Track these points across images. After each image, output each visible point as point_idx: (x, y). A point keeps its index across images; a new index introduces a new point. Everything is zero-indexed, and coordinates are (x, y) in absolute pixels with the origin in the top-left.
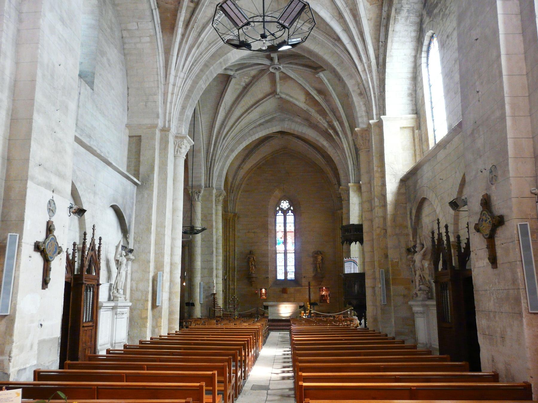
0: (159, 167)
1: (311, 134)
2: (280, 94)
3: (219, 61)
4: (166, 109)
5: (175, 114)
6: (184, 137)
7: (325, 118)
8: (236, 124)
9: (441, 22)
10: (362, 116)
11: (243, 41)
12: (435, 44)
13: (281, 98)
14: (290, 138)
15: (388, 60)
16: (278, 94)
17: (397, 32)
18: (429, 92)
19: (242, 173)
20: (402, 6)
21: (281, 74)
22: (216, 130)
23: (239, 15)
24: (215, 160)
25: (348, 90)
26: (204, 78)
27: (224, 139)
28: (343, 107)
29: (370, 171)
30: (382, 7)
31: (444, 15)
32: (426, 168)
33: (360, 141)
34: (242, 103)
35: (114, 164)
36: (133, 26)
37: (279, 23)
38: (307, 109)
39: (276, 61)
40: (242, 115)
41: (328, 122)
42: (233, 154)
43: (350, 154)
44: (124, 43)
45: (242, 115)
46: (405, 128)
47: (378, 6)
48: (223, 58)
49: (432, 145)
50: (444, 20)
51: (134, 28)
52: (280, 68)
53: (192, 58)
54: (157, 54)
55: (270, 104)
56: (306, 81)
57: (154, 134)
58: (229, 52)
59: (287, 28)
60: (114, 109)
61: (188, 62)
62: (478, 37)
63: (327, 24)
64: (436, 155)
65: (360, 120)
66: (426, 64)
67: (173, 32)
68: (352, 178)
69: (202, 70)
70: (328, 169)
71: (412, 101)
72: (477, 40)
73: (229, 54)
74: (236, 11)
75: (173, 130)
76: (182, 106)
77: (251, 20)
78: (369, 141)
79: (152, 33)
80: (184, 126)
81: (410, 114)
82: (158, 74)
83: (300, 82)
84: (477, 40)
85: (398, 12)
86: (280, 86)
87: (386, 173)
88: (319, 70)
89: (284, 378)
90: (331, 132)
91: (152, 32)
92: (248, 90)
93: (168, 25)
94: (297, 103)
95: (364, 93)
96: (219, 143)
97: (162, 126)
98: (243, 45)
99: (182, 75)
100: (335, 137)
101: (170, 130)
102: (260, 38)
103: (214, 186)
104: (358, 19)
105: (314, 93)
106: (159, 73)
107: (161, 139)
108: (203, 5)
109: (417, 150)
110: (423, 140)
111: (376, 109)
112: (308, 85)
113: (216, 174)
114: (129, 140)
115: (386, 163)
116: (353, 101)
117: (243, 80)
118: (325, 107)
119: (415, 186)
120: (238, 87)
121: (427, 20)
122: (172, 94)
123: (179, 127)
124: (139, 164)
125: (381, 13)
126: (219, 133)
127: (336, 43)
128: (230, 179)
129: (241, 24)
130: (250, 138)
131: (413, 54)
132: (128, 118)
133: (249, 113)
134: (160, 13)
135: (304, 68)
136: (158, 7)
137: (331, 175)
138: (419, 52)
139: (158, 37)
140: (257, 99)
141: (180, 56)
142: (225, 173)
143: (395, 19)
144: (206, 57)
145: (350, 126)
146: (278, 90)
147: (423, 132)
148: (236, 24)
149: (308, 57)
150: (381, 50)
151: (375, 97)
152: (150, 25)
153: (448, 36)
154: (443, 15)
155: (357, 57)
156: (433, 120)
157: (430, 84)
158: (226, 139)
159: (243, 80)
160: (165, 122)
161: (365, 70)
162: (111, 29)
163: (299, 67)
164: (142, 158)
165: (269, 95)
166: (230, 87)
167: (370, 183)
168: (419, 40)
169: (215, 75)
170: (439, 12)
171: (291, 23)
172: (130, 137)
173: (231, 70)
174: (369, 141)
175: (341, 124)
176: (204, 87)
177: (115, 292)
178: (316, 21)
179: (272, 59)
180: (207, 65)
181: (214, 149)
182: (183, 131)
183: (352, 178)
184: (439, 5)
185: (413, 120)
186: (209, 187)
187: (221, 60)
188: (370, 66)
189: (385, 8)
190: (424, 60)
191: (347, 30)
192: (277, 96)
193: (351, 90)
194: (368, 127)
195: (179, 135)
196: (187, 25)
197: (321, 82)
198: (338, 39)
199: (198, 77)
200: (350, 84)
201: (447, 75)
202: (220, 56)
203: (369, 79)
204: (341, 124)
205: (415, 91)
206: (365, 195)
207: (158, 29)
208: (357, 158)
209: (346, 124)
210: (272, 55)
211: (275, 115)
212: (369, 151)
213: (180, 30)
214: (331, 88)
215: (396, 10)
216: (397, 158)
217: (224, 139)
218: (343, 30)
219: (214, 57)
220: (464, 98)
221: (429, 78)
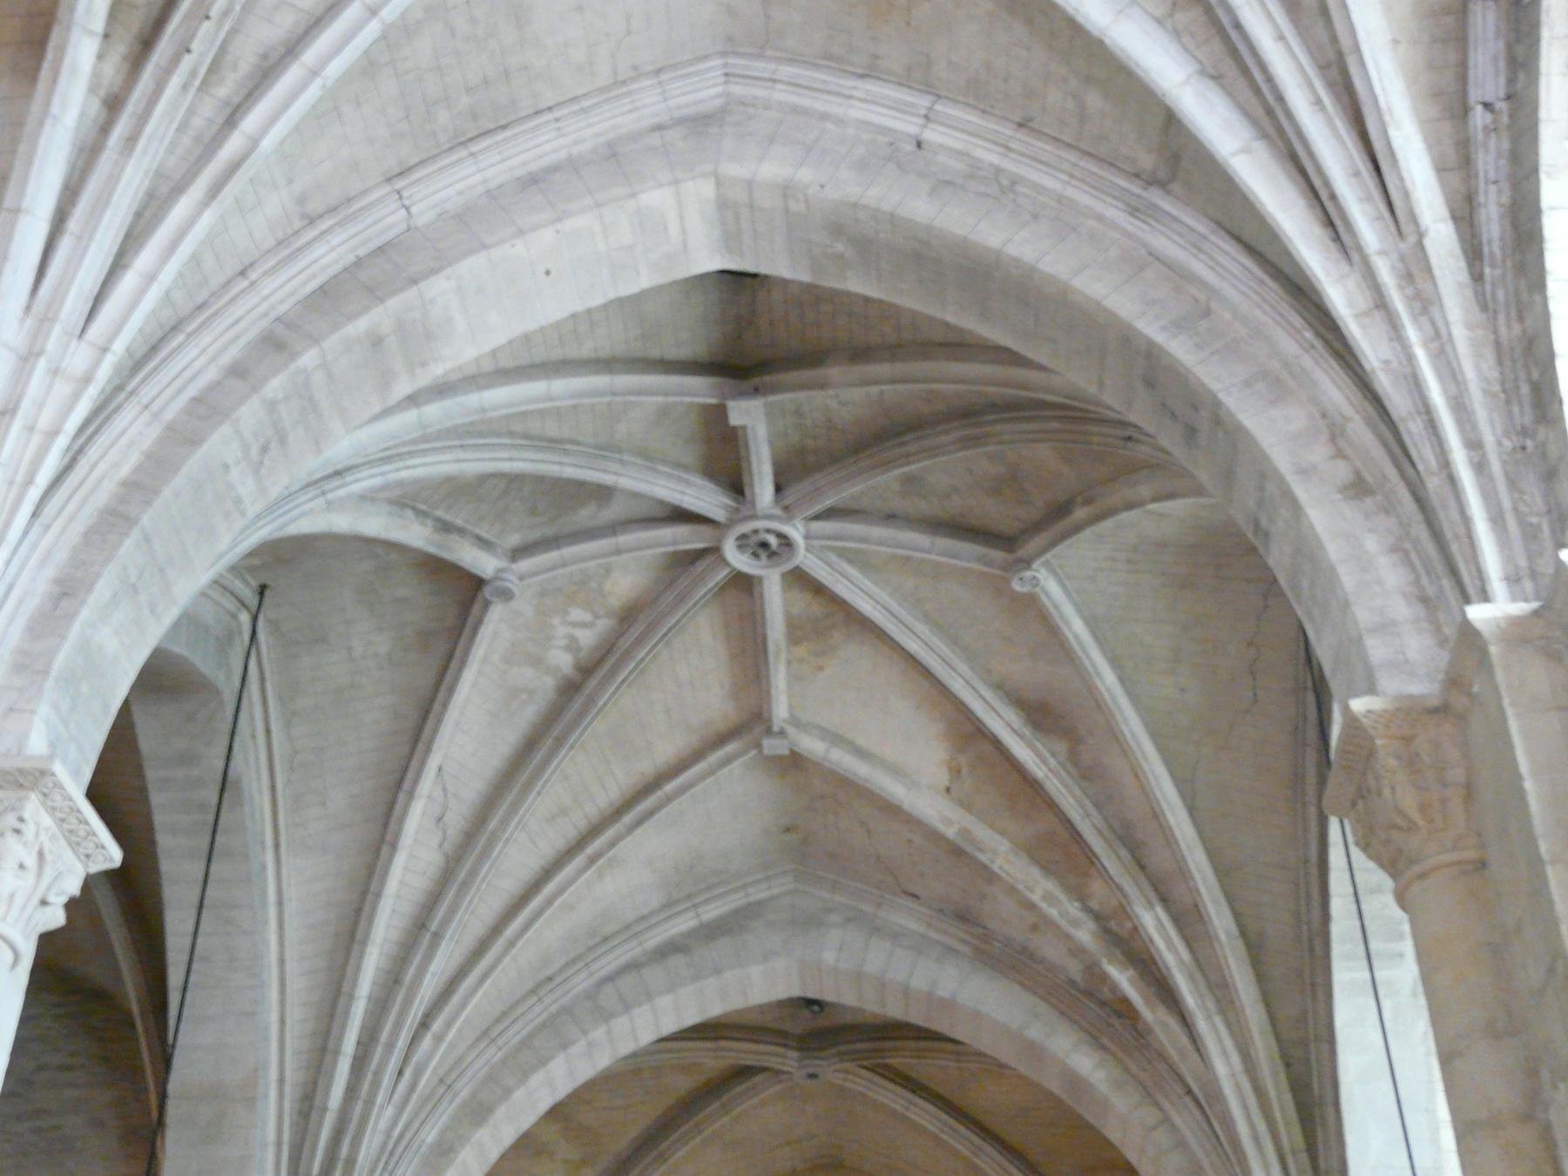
2: (790, 730)
3: (361, 326)
8: (510, 931)
10: (1386, 627)
16: (782, 733)
21: (803, 603)
27: (424, 1025)
28: (1192, 810)
38: (964, 832)
39: (763, 491)
40: (547, 874)
41: (1098, 917)
42: (483, 1134)
43: (1261, 1126)
45: (547, 874)
48: (393, 303)
55: (726, 811)
56: (954, 641)
67: (37, 69)
76: (58, 581)
80: (44, 709)
83: (913, 646)
86: (795, 679)
90: (1123, 979)
92: (591, 700)
94: (896, 790)
96: (390, 1046)
100: (1147, 1014)
105: (1004, 723)
112: (963, 668)
117: (561, 631)
120: (524, 675)
126: (393, 980)
130: (598, 1034)
135: (944, 543)
140: (646, 767)
141: (73, 225)
145: (1243, 933)
146: (780, 710)
151: (1480, 467)
158: (436, 1026)
165: (721, 740)
166: (469, 675)
175: (1188, 920)
188: (1416, 268)
194: (1454, 682)
202: (375, 294)
204: (1188, 920)
217: (424, 1025)
218: (1203, 72)
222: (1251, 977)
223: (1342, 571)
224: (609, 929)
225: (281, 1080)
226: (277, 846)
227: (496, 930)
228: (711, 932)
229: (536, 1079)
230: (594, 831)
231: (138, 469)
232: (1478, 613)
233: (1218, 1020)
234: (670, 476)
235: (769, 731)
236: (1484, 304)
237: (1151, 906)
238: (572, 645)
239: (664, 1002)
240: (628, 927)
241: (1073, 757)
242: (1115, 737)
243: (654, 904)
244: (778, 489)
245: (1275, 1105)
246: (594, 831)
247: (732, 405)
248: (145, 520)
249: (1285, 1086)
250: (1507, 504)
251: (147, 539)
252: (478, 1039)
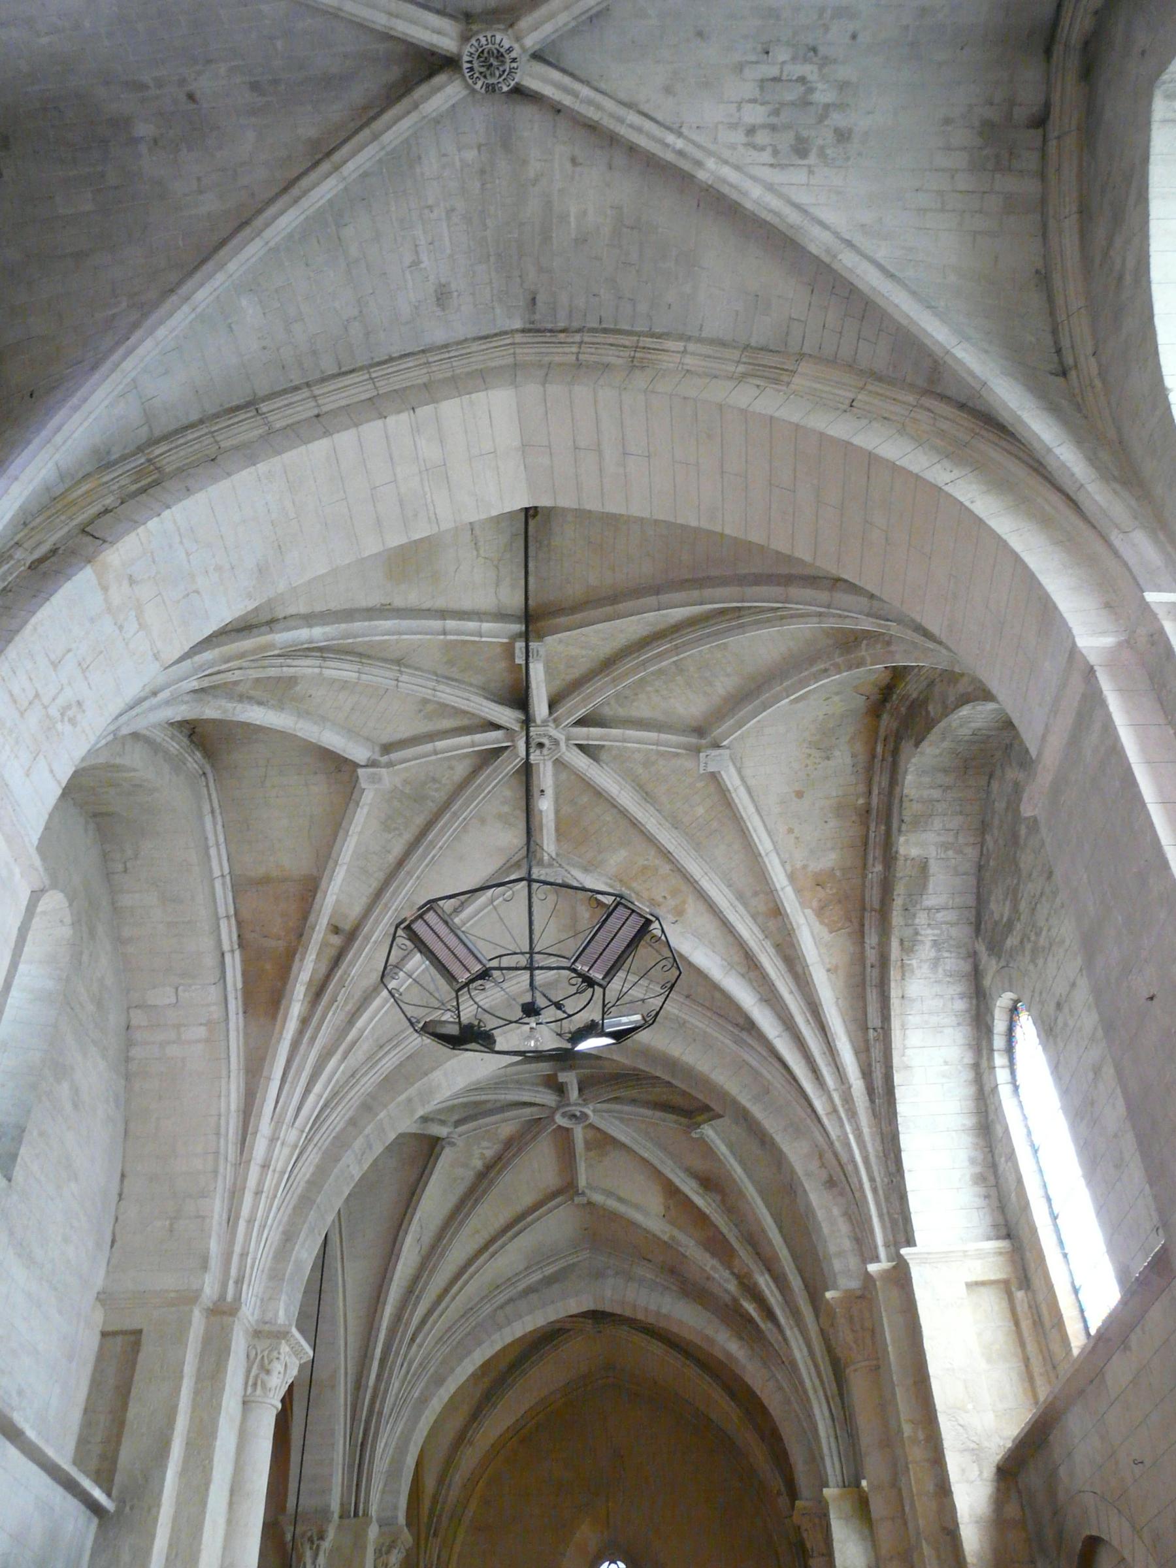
0: (189, 1444)
1: (687, 1318)
2: (587, 1191)
3: (404, 1096)
4: (231, 1242)
5: (261, 1253)
6: (282, 1335)
7: (729, 1267)
9: (1031, 967)
10: (841, 1254)
11: (470, 1026)
12: (1027, 1029)
13: (589, 1203)
14: (623, 1332)
15: (898, 1078)
16: (583, 1194)
17: (913, 1000)
18: (1035, 1168)
19: (470, 1458)
20: (917, 933)
21: (591, 1134)
22: (388, 1311)
23: (461, 951)
24: (380, 1413)
25: (793, 1172)
26: (358, 1143)
27: (413, 1340)
28: (780, 1228)
29: (890, 1441)
30: (863, 936)
31: (1034, 951)
32: (1076, 1425)
33: (844, 1335)
34: (473, 1222)
35: (31, 1434)
36: (162, 996)
37: (574, 971)
38: (673, 1238)
39: (574, 1094)
41: (738, 1277)
43: (817, 1383)
44: (130, 1044)
46: (983, 1284)
47: (849, 934)
49: (1077, 1341)
50: (1040, 962)
51: (167, 1001)
52: (585, 1116)
53: (326, 1087)
54: (224, 1073)
55: (556, 1226)
57: (184, 1325)
58: (433, 1069)
59: (600, 985)
60: (66, 1240)
61: (311, 1098)
62: (1153, 991)
63: (715, 987)
64: (1101, 1373)
65: (837, 1265)
66: (1009, 1088)
68: (832, 1468)
69: (352, 1122)
70: (747, 1438)
71: (987, 1197)
72: (1151, 998)
73: (437, 1075)
74: (452, 941)
75: (249, 1312)
76: (284, 1233)
77: (494, 963)
78: (873, 1331)
79: (215, 1016)
80: (284, 1297)
81: (989, 1239)
82: (218, 1134)
84: (1151, 998)
85: (909, 947)
87: (947, 1444)
88: (700, 1119)
90: (750, 1308)
91: (216, 1012)
92: (491, 1183)
93: (264, 995)
94: (638, 1217)
95: (839, 1179)
96: (397, 1353)
97: (215, 1297)
98: (471, 1036)
99: (292, 1136)
100: (762, 1325)
101: (237, 1309)
102: (520, 1014)
103: (373, 1510)
104: (799, 969)
105: (689, 1187)
106: (223, 1131)
107: (207, 1341)
108: (367, 939)
109: (1033, 1361)
110: (1048, 1325)
111: (883, 1227)
112: (670, 1162)
113: (381, 1464)
114: (101, 1347)
115: (938, 1407)
116: (808, 1205)
117: (477, 1152)
118: (725, 1230)
119: (1052, 1493)
121: (991, 965)
122: (258, 1193)
123: (267, 1301)
124: (119, 1437)
125: (863, 952)
126: (398, 1318)
127: (744, 1035)
128: (430, 1484)
129: (463, 977)
130: (496, 1336)
131: (969, 1058)
132: (108, 1272)
133: (492, 1256)
134: (245, 962)
135: (658, 1114)
136: (240, 945)
137: (759, 1456)
138: (985, 1052)
139: (232, 1025)
140: (519, 1208)
141: (289, 1079)
142: (411, 1461)
143: (902, 966)
144: (368, 1083)
145: (806, 1286)
146: (582, 1182)
147: (1040, 1297)
148: (449, 976)
149: (667, 1078)
150: (876, 1053)
151: (875, 1190)
152: (214, 993)
153: (1059, 1006)
154: (1034, 951)
155: (810, 1074)
156: (1065, 1255)
157: (1032, 1145)
158: (418, 1341)
159: (477, 1152)
160: (224, 1285)
161: (835, 1110)
162: (99, 1004)
163: (642, 1111)
164: (131, 1414)
166: (434, 1177)
167: (894, 1484)
168: (979, 1021)
169: (392, 1136)
170: (1022, 942)
171: (610, 973)
172: (104, 1334)
173: (443, 1122)
174: (875, 1332)
175: (780, 1281)
176: (357, 1172)
178: (677, 973)
179: (560, 1089)
180: (368, 1108)
181: (379, 1377)
182: (281, 1313)
183: (832, 1468)
184: (1018, 926)
185: (1001, 1259)
186: (356, 1514)
187: (412, 1091)
188: (848, 1099)
189: (872, 939)
190: (1002, 1075)
191: (771, 998)
192: (577, 1200)
193: (800, 1170)
195: (267, 1328)
196: (318, 991)
197: (708, 1151)
198: (750, 1026)
199: (340, 1143)
200: (796, 1153)
201: (1082, 1113)
203: (851, 1137)
204: (780, 1281)
205: (993, 1166)
206: (884, 1531)
207: (235, 1005)
208: (841, 1395)
209: (796, 1282)
210: (563, 1077)
211: (572, 1260)
212: (877, 1368)
213: (296, 1008)
214: (739, 1170)
215: (902, 941)
216: (975, 1396)
217: (413, 1340)
219: (390, 1084)
220: (1155, 1173)
221: (1027, 1126)
222: (810, 1309)
223: (824, 1225)
224: (499, 1282)
225: (346, 1373)
226: (342, 1258)
227: (446, 1291)
228: (549, 1281)
229: (467, 1361)
230: (493, 1240)
231: (313, 1174)
232: (872, 1268)
233: (796, 1329)
234: (529, 1090)
235: (577, 1193)
236: (875, 1115)
237: (763, 1274)
238: (482, 1156)
239: (528, 1318)
240: (509, 1279)
241: (723, 1201)
242: (741, 1194)
243: (521, 1267)
244: (580, 1090)
245: (823, 1372)
246: (493, 1240)
247: (559, 1074)
248: (318, 1200)
249: (828, 1363)
250: (885, 1211)
251: (318, 1207)
252: (437, 1343)
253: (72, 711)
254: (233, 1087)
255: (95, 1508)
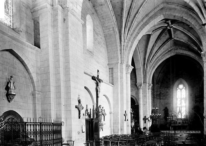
27: (150, 62)
39: (170, 23)
52: (172, 27)
89: (40, 5)
103: (147, 82)
122: (123, 49)
146: (173, 37)
177: (100, 66)
217: (150, 62)
253: (84, 139)
254: (118, 35)
255: (113, 87)
